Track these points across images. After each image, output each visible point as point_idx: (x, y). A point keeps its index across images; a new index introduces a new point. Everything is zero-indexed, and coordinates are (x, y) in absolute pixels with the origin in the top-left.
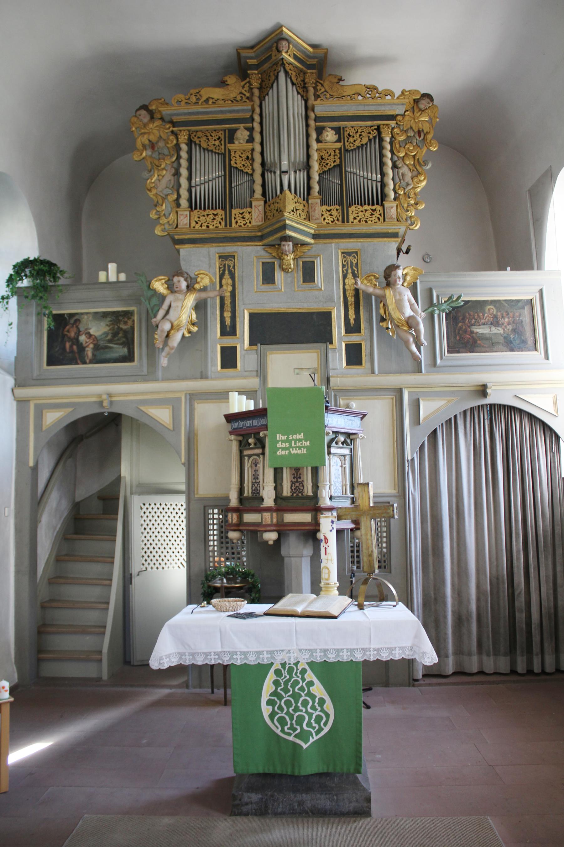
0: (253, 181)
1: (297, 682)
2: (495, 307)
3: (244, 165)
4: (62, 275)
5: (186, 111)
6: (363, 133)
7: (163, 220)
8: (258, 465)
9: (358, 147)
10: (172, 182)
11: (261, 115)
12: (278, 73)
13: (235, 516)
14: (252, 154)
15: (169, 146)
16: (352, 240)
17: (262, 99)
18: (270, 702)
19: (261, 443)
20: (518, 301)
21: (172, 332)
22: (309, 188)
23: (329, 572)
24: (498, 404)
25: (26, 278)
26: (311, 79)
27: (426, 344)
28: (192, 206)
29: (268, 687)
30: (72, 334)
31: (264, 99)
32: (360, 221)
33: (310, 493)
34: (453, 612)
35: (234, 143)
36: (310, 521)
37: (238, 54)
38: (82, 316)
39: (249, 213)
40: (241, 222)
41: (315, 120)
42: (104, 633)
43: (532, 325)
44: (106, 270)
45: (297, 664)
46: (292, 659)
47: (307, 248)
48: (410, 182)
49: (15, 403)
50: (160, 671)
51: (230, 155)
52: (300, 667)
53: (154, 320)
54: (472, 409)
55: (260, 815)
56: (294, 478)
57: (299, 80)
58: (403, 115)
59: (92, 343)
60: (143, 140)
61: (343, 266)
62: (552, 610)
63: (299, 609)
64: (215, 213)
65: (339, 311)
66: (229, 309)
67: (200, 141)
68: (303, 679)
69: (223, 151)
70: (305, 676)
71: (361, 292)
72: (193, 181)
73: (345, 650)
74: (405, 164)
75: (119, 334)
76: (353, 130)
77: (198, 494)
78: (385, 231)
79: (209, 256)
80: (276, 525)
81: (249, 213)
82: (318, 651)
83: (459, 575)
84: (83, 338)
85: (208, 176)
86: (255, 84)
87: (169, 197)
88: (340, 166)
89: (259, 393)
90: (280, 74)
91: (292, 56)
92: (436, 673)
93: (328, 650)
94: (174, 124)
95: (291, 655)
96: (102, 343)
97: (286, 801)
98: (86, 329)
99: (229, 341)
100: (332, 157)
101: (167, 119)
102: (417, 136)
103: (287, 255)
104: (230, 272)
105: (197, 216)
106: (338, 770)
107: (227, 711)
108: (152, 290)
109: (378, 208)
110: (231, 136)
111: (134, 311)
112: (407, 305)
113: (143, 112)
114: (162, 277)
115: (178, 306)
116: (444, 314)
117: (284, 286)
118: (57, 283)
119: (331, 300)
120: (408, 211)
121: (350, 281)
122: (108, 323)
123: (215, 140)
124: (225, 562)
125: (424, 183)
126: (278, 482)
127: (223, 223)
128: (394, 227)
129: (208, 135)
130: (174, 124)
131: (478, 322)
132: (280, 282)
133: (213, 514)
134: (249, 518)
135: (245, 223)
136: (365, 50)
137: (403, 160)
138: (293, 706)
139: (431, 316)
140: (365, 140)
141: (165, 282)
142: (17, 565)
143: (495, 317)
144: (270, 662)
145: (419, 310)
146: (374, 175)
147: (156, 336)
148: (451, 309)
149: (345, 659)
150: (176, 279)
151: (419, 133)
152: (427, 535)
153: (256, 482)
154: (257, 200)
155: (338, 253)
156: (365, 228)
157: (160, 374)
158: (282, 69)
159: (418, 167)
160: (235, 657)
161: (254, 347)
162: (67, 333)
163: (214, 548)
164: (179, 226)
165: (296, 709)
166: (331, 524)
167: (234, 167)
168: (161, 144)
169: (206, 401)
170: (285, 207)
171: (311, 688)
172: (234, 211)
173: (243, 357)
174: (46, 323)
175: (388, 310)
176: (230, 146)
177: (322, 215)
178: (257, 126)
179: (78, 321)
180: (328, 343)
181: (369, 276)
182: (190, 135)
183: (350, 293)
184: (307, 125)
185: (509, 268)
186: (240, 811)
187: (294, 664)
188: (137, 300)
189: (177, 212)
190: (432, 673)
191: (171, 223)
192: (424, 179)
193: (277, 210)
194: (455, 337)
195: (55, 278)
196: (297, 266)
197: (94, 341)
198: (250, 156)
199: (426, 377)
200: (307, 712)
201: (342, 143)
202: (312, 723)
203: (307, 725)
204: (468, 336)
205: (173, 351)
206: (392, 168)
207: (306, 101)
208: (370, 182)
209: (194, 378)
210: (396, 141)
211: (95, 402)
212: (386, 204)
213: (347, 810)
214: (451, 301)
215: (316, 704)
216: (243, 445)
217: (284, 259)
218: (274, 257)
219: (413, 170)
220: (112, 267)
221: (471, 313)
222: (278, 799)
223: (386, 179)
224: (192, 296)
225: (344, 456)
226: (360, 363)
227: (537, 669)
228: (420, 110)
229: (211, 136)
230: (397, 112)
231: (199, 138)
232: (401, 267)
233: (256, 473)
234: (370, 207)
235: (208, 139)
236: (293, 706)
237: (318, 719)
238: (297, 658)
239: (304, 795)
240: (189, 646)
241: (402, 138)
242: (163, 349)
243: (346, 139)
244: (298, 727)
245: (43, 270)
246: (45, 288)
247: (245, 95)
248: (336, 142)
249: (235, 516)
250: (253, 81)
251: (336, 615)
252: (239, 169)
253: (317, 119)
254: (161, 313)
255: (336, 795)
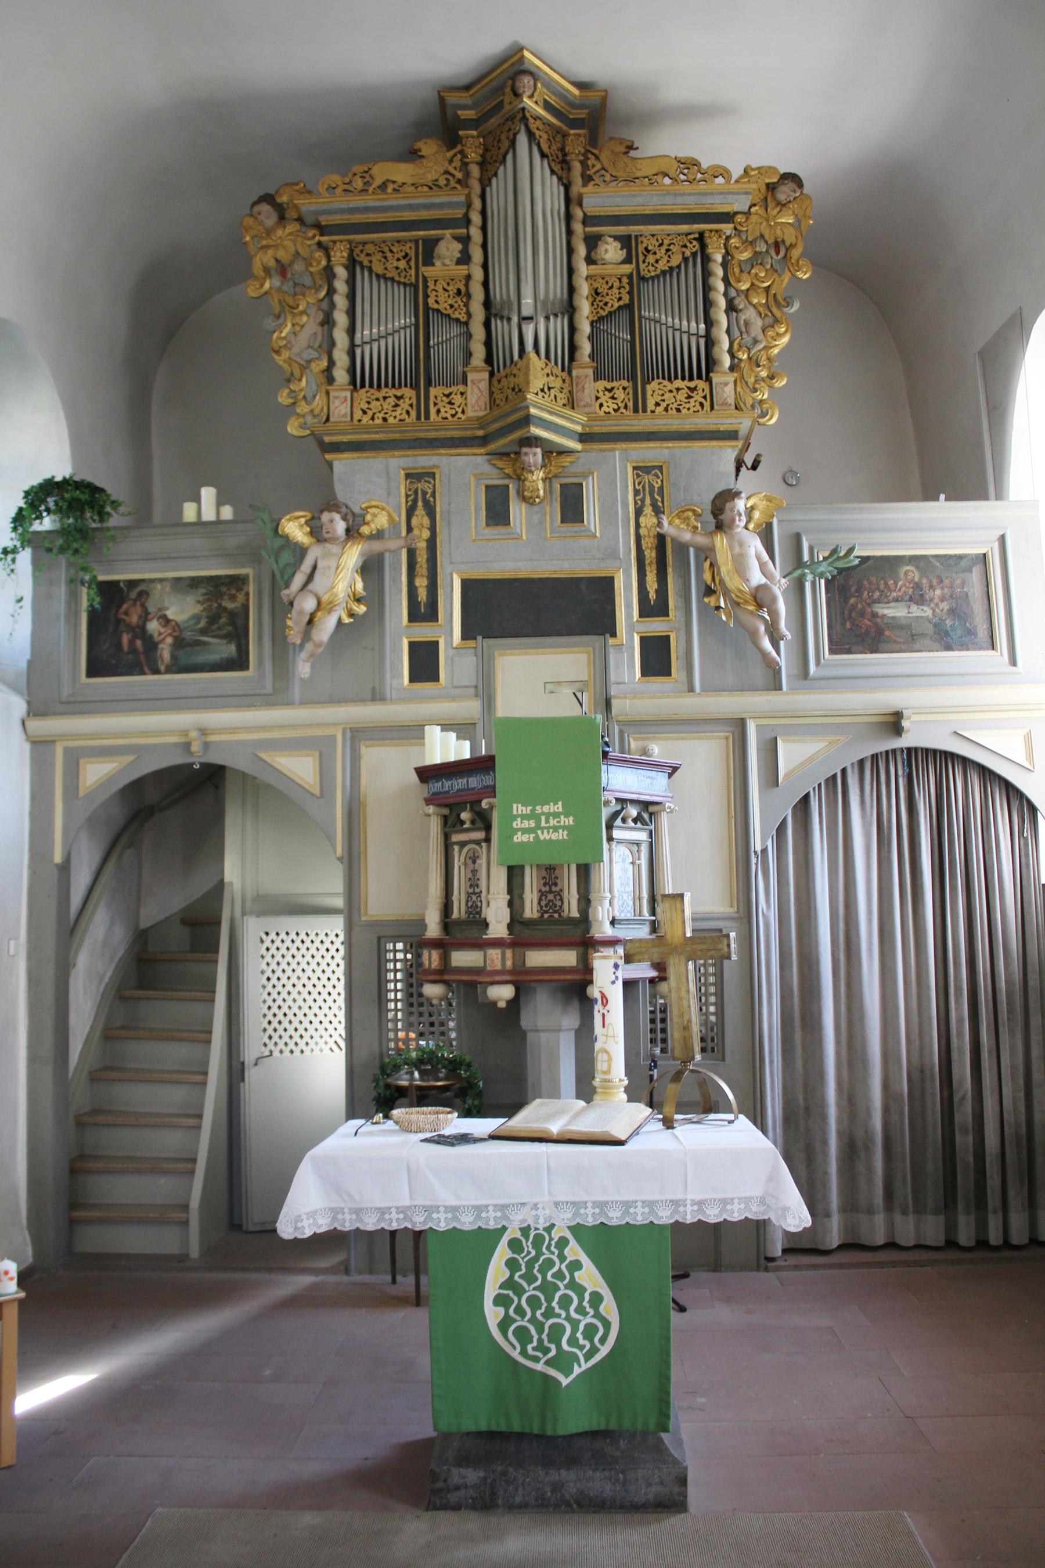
0: (469, 336)
1: (550, 1263)
2: (917, 567)
3: (451, 306)
4: (115, 509)
5: (345, 206)
6: (672, 247)
7: (303, 408)
8: (478, 861)
9: (664, 272)
10: (319, 337)
11: (483, 213)
12: (515, 135)
13: (435, 955)
14: (467, 286)
15: (312, 270)
16: (651, 444)
17: (485, 183)
18: (500, 1300)
19: (483, 821)
20: (960, 557)
21: (319, 614)
22: (573, 348)
23: (610, 1060)
24: (922, 749)
25: (49, 514)
26: (576, 146)
27: (789, 637)
28: (356, 382)
29: (496, 1273)
30: (134, 619)
31: (490, 184)
32: (666, 409)
33: (575, 913)
34: (840, 1133)
35: (433, 265)
36: (575, 964)
37: (442, 100)
38: (153, 585)
39: (462, 394)
40: (447, 411)
41: (584, 223)
42: (192, 1172)
43: (986, 602)
44: (197, 499)
45: (549, 1229)
46: (541, 1221)
47: (569, 459)
48: (760, 336)
49: (27, 747)
50: (296, 1243)
51: (426, 287)
52: (556, 1235)
53: (286, 592)
54: (875, 757)
55: (482, 1508)
56: (545, 885)
57: (554, 147)
58: (748, 214)
59: (170, 635)
60: (265, 260)
61: (636, 492)
62: (1023, 1130)
63: (555, 1128)
64: (399, 394)
65: (628, 576)
66: (425, 572)
67: (371, 262)
68: (562, 1258)
69: (413, 280)
70: (566, 1252)
71: (668, 540)
72: (358, 335)
73: (639, 1204)
74: (750, 303)
75: (220, 618)
76: (653, 241)
77: (366, 914)
78: (713, 428)
79: (388, 473)
80: (511, 972)
81: (462, 394)
82: (589, 1205)
83: (851, 1064)
84: (153, 626)
85: (385, 325)
86: (473, 156)
87: (313, 365)
88: (629, 307)
89: (479, 728)
90: (518, 137)
91: (541, 104)
92: (809, 1246)
93: (607, 1202)
94: (322, 230)
95: (538, 1212)
96: (188, 635)
97: (529, 1483)
98: (160, 610)
99: (424, 632)
100: (615, 290)
101: (309, 220)
102: (773, 252)
103: (532, 472)
104: (426, 503)
105: (365, 400)
106: (627, 1425)
107: (420, 1316)
108: (281, 536)
109: (701, 384)
110: (428, 252)
111: (247, 575)
112: (754, 565)
113: (265, 208)
114: (301, 513)
115: (329, 567)
116: (823, 581)
117: (527, 530)
118: (105, 525)
119: (613, 554)
120: (755, 390)
121: (648, 520)
122: (200, 599)
123: (398, 260)
124: (417, 1040)
125: (785, 340)
126: (516, 892)
127: (413, 413)
128: (729, 421)
129: (386, 249)
130: (322, 230)
131: (887, 597)
132: (518, 522)
133: (395, 951)
134: (461, 958)
135: (454, 412)
136: (676, 92)
137: (747, 296)
138: (543, 1307)
139: (799, 586)
140: (676, 260)
141: (306, 523)
142: (31, 1047)
143: (917, 586)
144: (500, 1226)
145: (777, 574)
146: (693, 324)
147: (289, 623)
148: (835, 572)
149: (640, 1220)
150: (325, 517)
151: (777, 245)
152: (791, 990)
153: (474, 893)
154: (476, 370)
155: (626, 468)
156: (677, 422)
157: (296, 692)
158: (523, 128)
159: (774, 310)
160: (435, 1216)
161: (471, 643)
162: (124, 617)
163: (396, 1015)
164: (332, 419)
165: (549, 1313)
166: (614, 970)
167: (434, 310)
168: (299, 267)
169: (381, 742)
170: (528, 383)
171: (576, 1274)
172: (433, 391)
173: (451, 661)
174: (85, 597)
175: (719, 573)
176: (427, 271)
177: (597, 398)
178: (475, 233)
179: (144, 595)
180: (608, 635)
181: (683, 512)
182: (351, 251)
183: (648, 543)
184: (569, 232)
185: (942, 496)
186: (445, 1501)
187: (544, 1229)
188: (254, 556)
189: (328, 393)
190: (800, 1247)
191: (316, 412)
192: (786, 332)
193: (513, 389)
194: (843, 624)
195: (102, 515)
196: (551, 492)
197: (174, 631)
198: (463, 289)
199: (790, 699)
200: (568, 1318)
201: (633, 266)
202: (578, 1339)
203: (569, 1342)
204: (867, 622)
205: (321, 650)
206: (726, 312)
207: (567, 188)
208: (685, 337)
209: (359, 700)
210: (735, 262)
211: (176, 745)
212: (716, 378)
213: (644, 1500)
214: (835, 556)
215: (585, 1304)
216: (450, 824)
217: (526, 479)
218: (508, 476)
219: (766, 315)
220: (208, 494)
221: (873, 579)
222: (514, 1479)
223: (714, 332)
224: (355, 548)
225: (638, 844)
226: (667, 672)
227: (995, 1238)
228: (779, 203)
229: (391, 251)
230: (736, 208)
231: (368, 255)
232: (743, 495)
233: (474, 875)
234: (686, 383)
235: (386, 258)
236: (543, 1307)
237: (590, 1331)
238: (551, 1217)
239: (563, 1472)
240: (350, 1196)
241: (745, 256)
242: (302, 646)
243: (641, 258)
244: (553, 1347)
245: (79, 500)
246: (83, 533)
247: (453, 176)
248: (623, 262)
249: (435, 955)
250: (468, 151)
251: (623, 1139)
252: (442, 314)
253: (587, 221)
254: (299, 579)
255: (623, 1472)
